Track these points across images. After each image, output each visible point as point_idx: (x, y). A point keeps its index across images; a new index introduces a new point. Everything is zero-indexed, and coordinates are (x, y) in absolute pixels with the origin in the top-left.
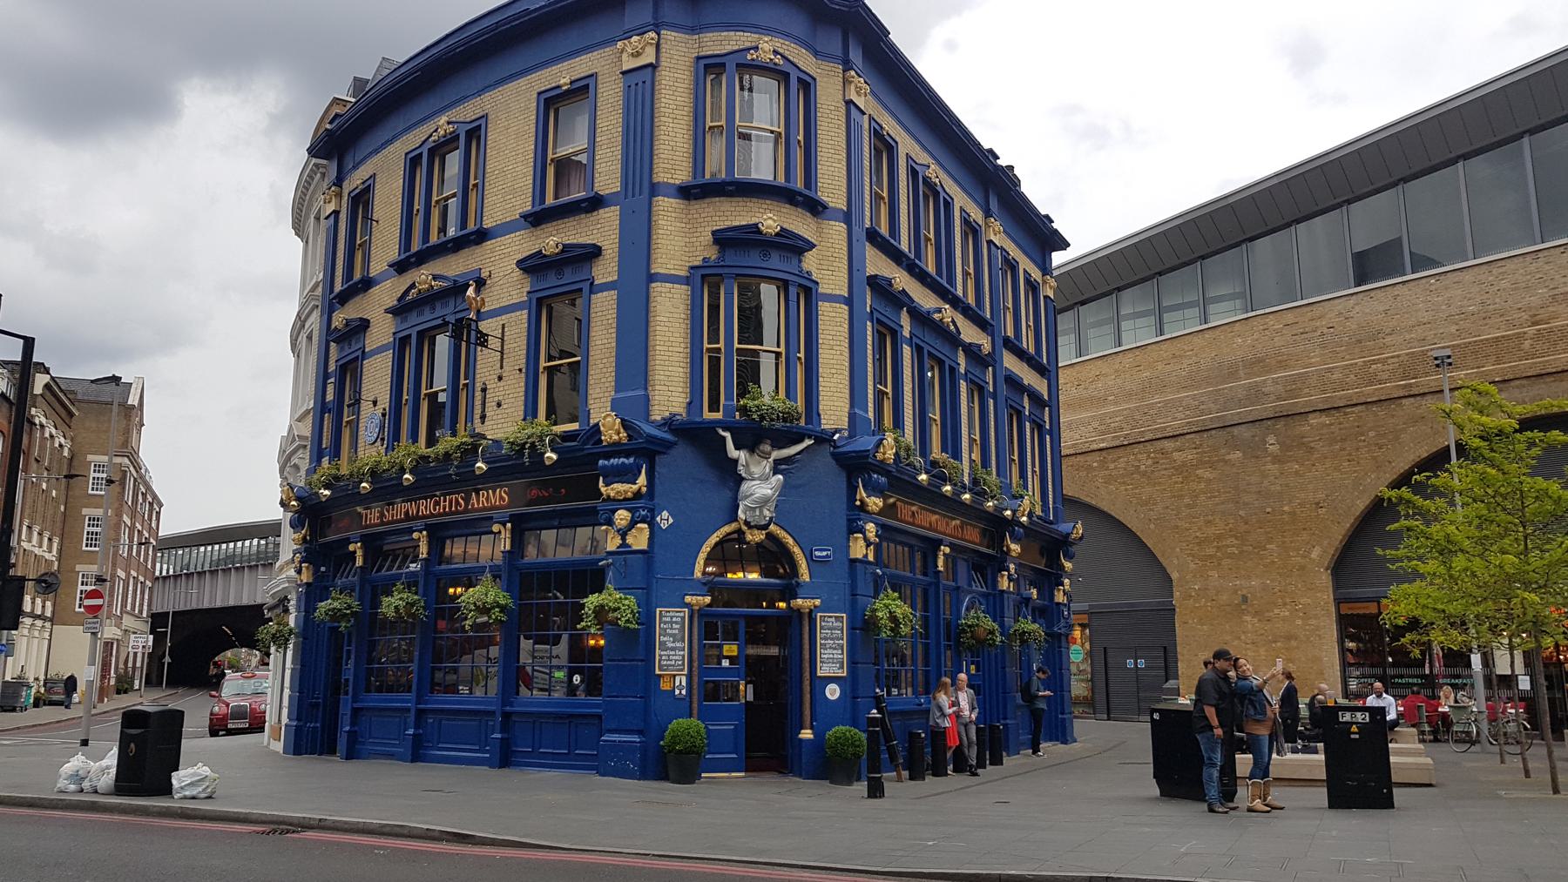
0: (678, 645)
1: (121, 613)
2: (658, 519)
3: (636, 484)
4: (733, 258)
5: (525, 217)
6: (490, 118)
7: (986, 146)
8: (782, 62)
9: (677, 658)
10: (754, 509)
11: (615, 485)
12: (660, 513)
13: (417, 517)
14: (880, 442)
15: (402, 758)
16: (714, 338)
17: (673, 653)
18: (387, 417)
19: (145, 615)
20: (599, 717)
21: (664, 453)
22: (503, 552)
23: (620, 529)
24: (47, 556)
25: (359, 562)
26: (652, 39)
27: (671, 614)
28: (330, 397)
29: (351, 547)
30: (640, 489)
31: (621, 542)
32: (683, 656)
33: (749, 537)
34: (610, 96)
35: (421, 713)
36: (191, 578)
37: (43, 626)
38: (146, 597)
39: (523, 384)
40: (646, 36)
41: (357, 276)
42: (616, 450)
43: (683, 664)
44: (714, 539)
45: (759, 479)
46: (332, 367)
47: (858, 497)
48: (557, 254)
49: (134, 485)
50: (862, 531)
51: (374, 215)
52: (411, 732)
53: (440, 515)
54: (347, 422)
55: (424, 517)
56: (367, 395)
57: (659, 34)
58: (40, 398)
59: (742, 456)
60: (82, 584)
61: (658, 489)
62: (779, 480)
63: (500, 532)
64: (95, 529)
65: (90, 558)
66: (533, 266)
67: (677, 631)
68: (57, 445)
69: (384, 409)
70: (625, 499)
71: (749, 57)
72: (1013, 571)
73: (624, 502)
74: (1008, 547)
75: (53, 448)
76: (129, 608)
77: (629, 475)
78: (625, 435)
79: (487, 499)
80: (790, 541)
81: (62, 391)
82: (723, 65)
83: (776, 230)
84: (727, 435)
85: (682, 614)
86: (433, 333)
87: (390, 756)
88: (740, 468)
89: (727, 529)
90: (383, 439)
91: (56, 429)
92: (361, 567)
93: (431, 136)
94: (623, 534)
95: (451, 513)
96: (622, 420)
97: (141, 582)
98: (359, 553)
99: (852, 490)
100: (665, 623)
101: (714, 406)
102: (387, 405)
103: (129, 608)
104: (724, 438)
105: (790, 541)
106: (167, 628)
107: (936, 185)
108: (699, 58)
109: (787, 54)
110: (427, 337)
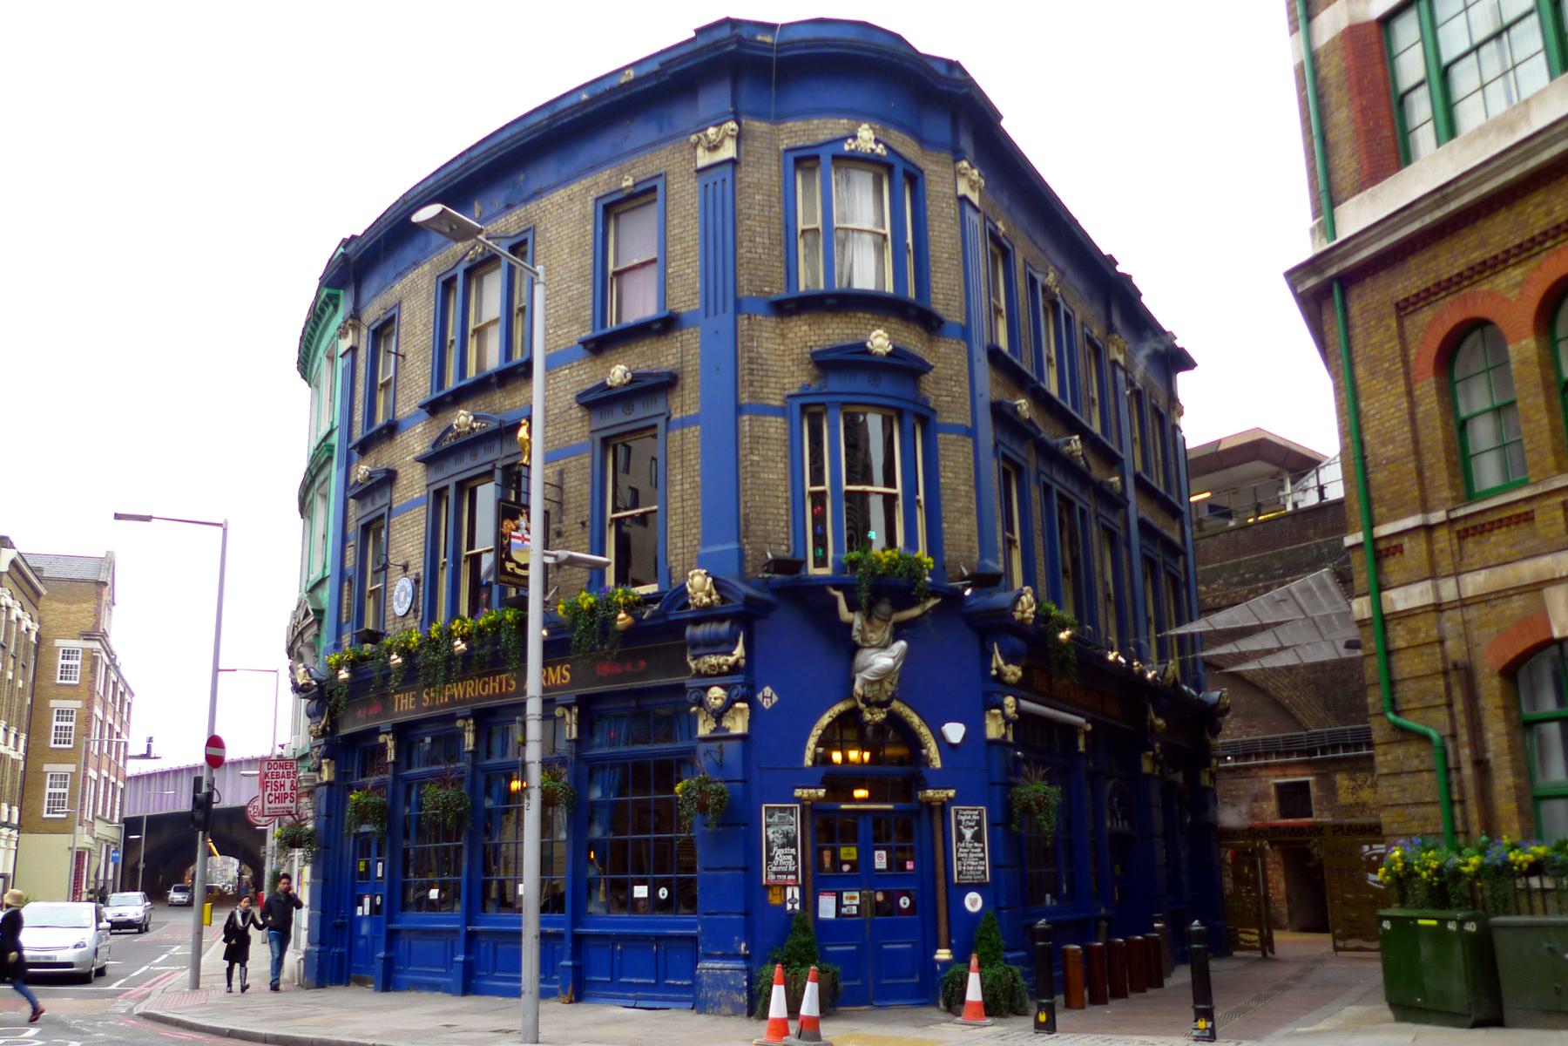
1: (93, 819)
3: (732, 655)
5: (584, 343)
6: (538, 230)
7: (1105, 252)
8: (885, 153)
11: (707, 659)
12: (761, 689)
15: (446, 989)
16: (817, 478)
18: (421, 583)
19: (116, 820)
20: (694, 939)
22: (569, 741)
23: (714, 710)
24: (13, 755)
25: (391, 757)
26: (732, 130)
28: (349, 564)
29: (381, 739)
30: (737, 661)
31: (715, 725)
33: (868, 717)
34: (685, 197)
35: (471, 937)
36: (166, 777)
38: (118, 800)
39: (587, 540)
41: (380, 420)
42: (707, 615)
44: (826, 720)
46: (351, 530)
47: (994, 665)
48: (626, 385)
49: (106, 673)
50: (1001, 706)
51: (400, 349)
52: (460, 958)
53: (489, 697)
54: (371, 592)
55: (472, 700)
56: (395, 559)
57: (739, 124)
58: (5, 577)
59: (857, 620)
60: (51, 787)
63: (564, 716)
64: (64, 724)
65: (61, 756)
66: (597, 401)
68: (24, 629)
69: (417, 574)
70: (721, 674)
71: (846, 148)
72: (1158, 751)
73: (717, 674)
74: (1152, 721)
75: (19, 633)
76: (100, 813)
77: (722, 645)
78: (718, 597)
81: (30, 568)
82: (816, 158)
84: (839, 595)
86: (472, 484)
87: (433, 987)
88: (855, 633)
89: (840, 708)
90: (416, 611)
91: (23, 610)
93: (467, 254)
94: (719, 715)
95: (502, 696)
96: (715, 580)
97: (105, 778)
98: (390, 744)
99: (987, 657)
101: (821, 562)
102: (421, 570)
103: (100, 813)
104: (835, 599)
107: (1056, 296)
109: (891, 143)
110: (467, 489)
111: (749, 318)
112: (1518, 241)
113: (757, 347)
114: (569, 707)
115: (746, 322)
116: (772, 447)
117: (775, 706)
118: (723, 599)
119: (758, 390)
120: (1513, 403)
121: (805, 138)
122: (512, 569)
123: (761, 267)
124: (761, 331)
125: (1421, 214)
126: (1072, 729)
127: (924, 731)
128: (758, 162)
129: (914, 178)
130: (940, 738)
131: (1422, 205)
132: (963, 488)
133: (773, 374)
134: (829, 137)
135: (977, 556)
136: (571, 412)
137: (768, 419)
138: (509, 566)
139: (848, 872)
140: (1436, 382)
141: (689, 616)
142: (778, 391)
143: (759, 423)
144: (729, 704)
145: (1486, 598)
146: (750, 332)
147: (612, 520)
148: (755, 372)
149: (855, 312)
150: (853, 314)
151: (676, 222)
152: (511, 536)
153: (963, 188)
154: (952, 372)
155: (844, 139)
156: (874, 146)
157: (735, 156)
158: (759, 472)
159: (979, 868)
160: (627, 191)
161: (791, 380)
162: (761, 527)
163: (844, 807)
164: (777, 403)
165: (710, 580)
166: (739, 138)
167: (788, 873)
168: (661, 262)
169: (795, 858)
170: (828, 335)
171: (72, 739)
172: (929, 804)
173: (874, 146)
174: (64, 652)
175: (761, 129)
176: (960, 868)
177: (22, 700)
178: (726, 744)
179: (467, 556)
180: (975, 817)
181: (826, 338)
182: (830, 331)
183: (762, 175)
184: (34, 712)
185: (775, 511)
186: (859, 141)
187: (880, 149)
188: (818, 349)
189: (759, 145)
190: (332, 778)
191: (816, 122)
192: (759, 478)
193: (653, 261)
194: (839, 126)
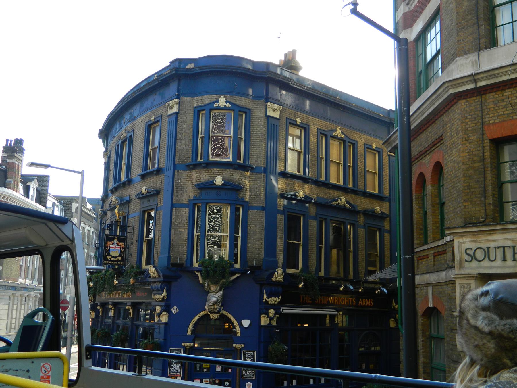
8: (230, 106)
10: (211, 306)
12: (173, 307)
14: (273, 273)
25: (131, 315)
30: (164, 297)
40: (174, 100)
44: (196, 318)
47: (264, 298)
50: (267, 314)
70: (160, 301)
71: (215, 106)
74: (394, 306)
83: (222, 183)
92: (131, 317)
98: (131, 310)
104: (198, 276)
106: (325, 316)
111: (178, 171)
113: (180, 182)
115: (177, 173)
117: (177, 313)
119: (179, 198)
121: (201, 103)
122: (110, 258)
123: (184, 152)
124: (182, 176)
127: (235, 322)
128: (185, 113)
130: (241, 325)
132: (258, 230)
134: (209, 102)
137: (183, 209)
138: (108, 257)
139: (206, 372)
142: (187, 198)
146: (178, 177)
148: (179, 192)
150: (212, 169)
153: (270, 113)
155: (214, 103)
156: (225, 104)
157: (178, 111)
158: (177, 229)
159: (252, 373)
160: (153, 121)
162: (177, 249)
164: (186, 203)
165: (154, 269)
166: (179, 104)
167: (177, 372)
169: (180, 367)
170: (204, 177)
173: (225, 104)
176: (244, 373)
179: (146, 240)
180: (252, 355)
181: (203, 178)
182: (204, 176)
183: (188, 118)
191: (205, 96)
192: (177, 231)
194: (210, 98)
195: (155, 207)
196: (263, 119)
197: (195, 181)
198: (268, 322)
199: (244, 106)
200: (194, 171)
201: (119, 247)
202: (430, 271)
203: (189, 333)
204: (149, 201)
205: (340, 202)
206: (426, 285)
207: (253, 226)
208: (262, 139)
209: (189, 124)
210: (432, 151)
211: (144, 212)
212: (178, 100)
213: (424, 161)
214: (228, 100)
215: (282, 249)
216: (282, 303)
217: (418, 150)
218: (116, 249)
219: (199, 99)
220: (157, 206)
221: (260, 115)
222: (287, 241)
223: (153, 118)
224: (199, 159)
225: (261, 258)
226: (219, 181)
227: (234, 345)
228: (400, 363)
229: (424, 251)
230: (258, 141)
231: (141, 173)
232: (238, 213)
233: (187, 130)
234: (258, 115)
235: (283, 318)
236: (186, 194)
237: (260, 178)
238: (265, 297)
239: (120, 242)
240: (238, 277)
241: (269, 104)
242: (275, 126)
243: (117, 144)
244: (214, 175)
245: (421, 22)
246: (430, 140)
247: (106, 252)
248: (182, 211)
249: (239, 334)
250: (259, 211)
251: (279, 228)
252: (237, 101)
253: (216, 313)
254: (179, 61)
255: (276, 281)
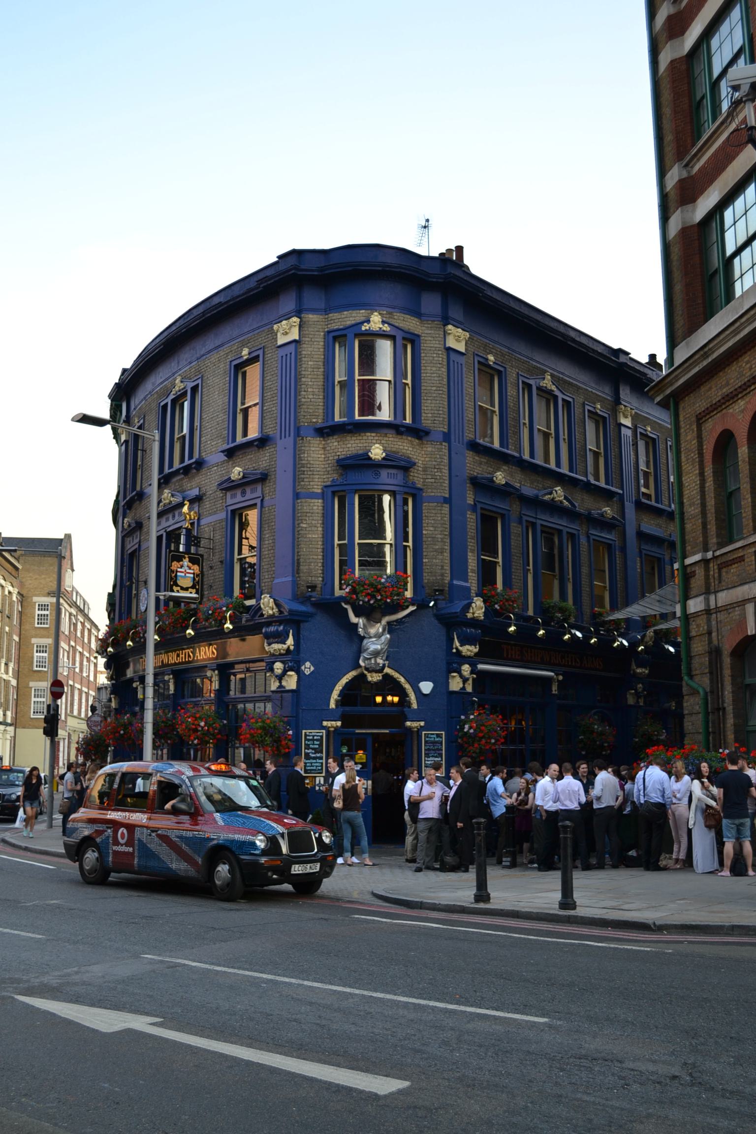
0: (318, 755)
2: (303, 668)
4: (355, 477)
8: (388, 329)
9: (317, 764)
10: (370, 659)
12: (304, 664)
13: (168, 665)
14: (469, 606)
17: (315, 761)
21: (307, 621)
27: (313, 734)
29: (134, 685)
30: (289, 647)
31: (278, 684)
32: (322, 763)
37: (5, 730)
40: (291, 320)
43: (322, 769)
45: (375, 637)
47: (454, 646)
48: (240, 479)
50: (459, 672)
53: (180, 663)
59: (361, 621)
61: (303, 646)
62: (387, 638)
67: (317, 746)
68: (7, 593)
70: (281, 654)
71: (363, 328)
74: (634, 671)
77: (281, 638)
79: (205, 653)
80: (402, 680)
83: (383, 456)
84: (349, 608)
85: (321, 734)
94: (280, 678)
96: (275, 600)
100: (309, 740)
104: (346, 610)
105: (402, 680)
108: (329, 332)
112: (739, 384)
114: (214, 670)
116: (315, 518)
117: (312, 673)
118: (281, 612)
119: (307, 483)
120: (739, 488)
125: (696, 363)
126: (549, 680)
127: (407, 686)
129: (413, 339)
130: (417, 691)
131: (697, 357)
132: (439, 536)
133: (317, 473)
134: (353, 322)
135: (449, 578)
136: (217, 493)
137: (313, 501)
140: (713, 468)
141: (263, 620)
143: (307, 504)
144: (285, 672)
145: (726, 608)
147: (238, 559)
148: (306, 473)
149: (365, 432)
150: (363, 434)
151: (268, 378)
152: (177, 571)
153: (451, 343)
154: (435, 463)
155: (362, 323)
161: (328, 476)
162: (307, 567)
163: (357, 731)
168: (260, 404)
171: (47, 665)
172: (410, 729)
174: (39, 605)
175: (313, 320)
177: (10, 639)
178: (284, 695)
181: (347, 449)
182: (350, 445)
183: (314, 349)
184: (22, 646)
185: (316, 557)
186: (372, 323)
187: (386, 328)
188: (343, 456)
189: (312, 330)
190: (117, 707)
191: (345, 313)
193: (257, 404)
195: (258, 501)
196: (440, 352)
197: (333, 454)
198: (461, 685)
199: (411, 331)
200: (331, 438)
201: (192, 571)
202: (736, 584)
203: (332, 705)
204: (244, 493)
205: (555, 495)
206: (742, 603)
207: (432, 529)
208: (440, 385)
209: (317, 360)
210: (749, 393)
211: (233, 512)
212: (298, 320)
213: (731, 411)
214: (385, 319)
215: (474, 568)
216: (482, 656)
217: (720, 393)
218: (187, 575)
219: (335, 318)
220: (262, 500)
221: (435, 346)
222: (482, 557)
223: (245, 352)
224: (337, 418)
225: (446, 582)
226: (377, 452)
227: (408, 724)
228: (685, 736)
229: (735, 552)
230: (434, 388)
231: (226, 447)
232: (406, 508)
233: (315, 370)
234: (432, 345)
235: (481, 678)
236: (317, 476)
237: (440, 450)
238: (457, 643)
239: (193, 564)
240: (412, 612)
241: (450, 327)
242: (460, 365)
243: (162, 404)
244: (367, 444)
245: (716, 193)
246: (748, 374)
247: (172, 579)
248: (312, 504)
249: (415, 706)
250: (439, 505)
251: (470, 533)
252: (399, 321)
253: (377, 671)
254: (296, 254)
255: (473, 619)
